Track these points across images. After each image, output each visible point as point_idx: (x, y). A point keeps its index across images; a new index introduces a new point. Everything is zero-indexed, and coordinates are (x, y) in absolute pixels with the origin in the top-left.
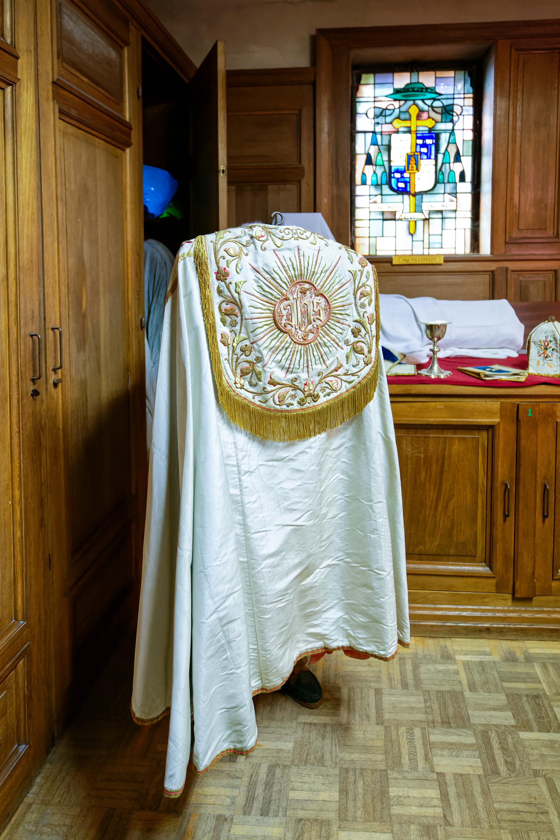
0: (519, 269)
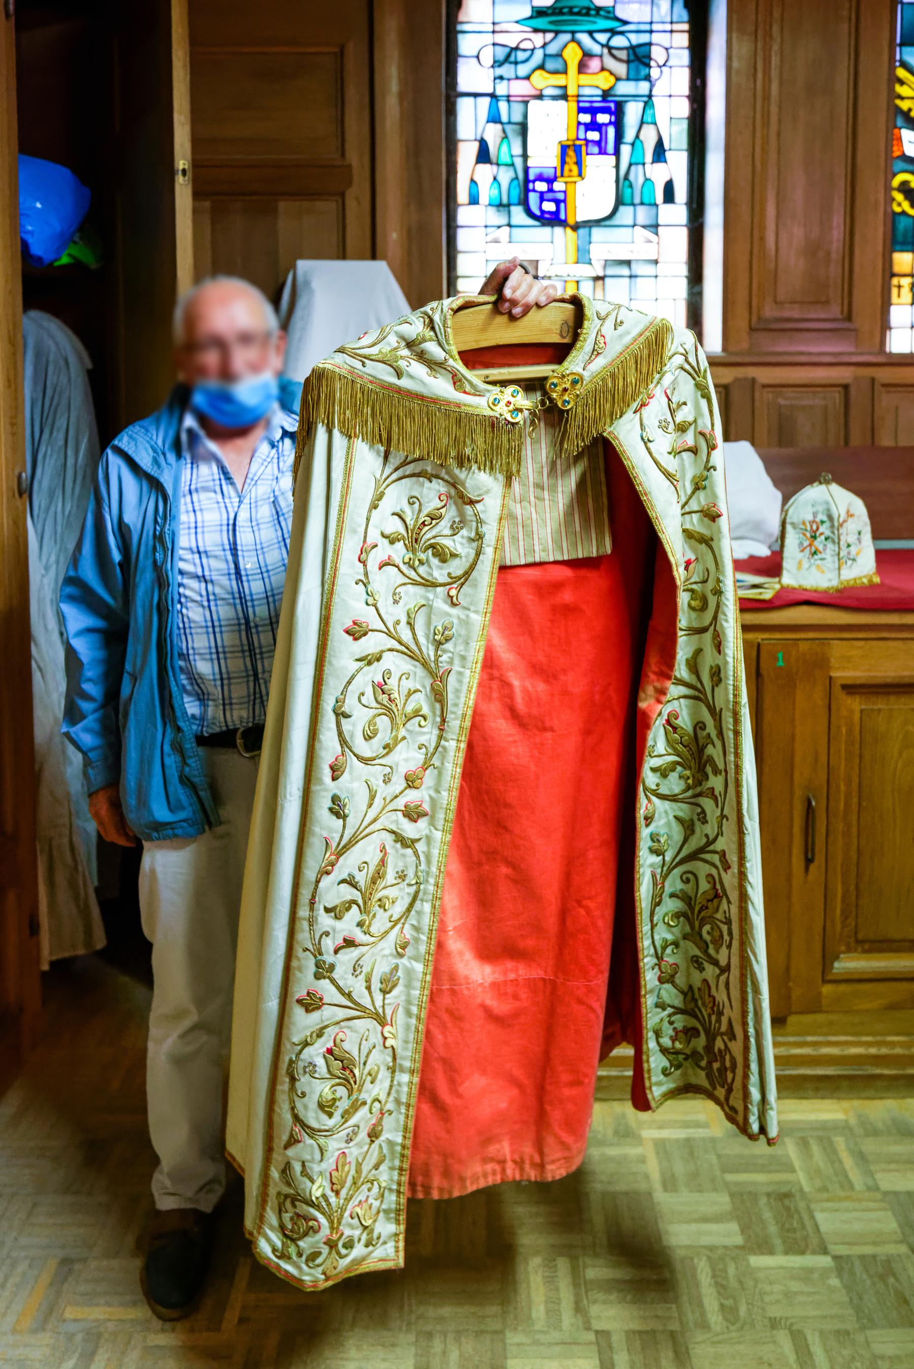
0: (778, 381)
